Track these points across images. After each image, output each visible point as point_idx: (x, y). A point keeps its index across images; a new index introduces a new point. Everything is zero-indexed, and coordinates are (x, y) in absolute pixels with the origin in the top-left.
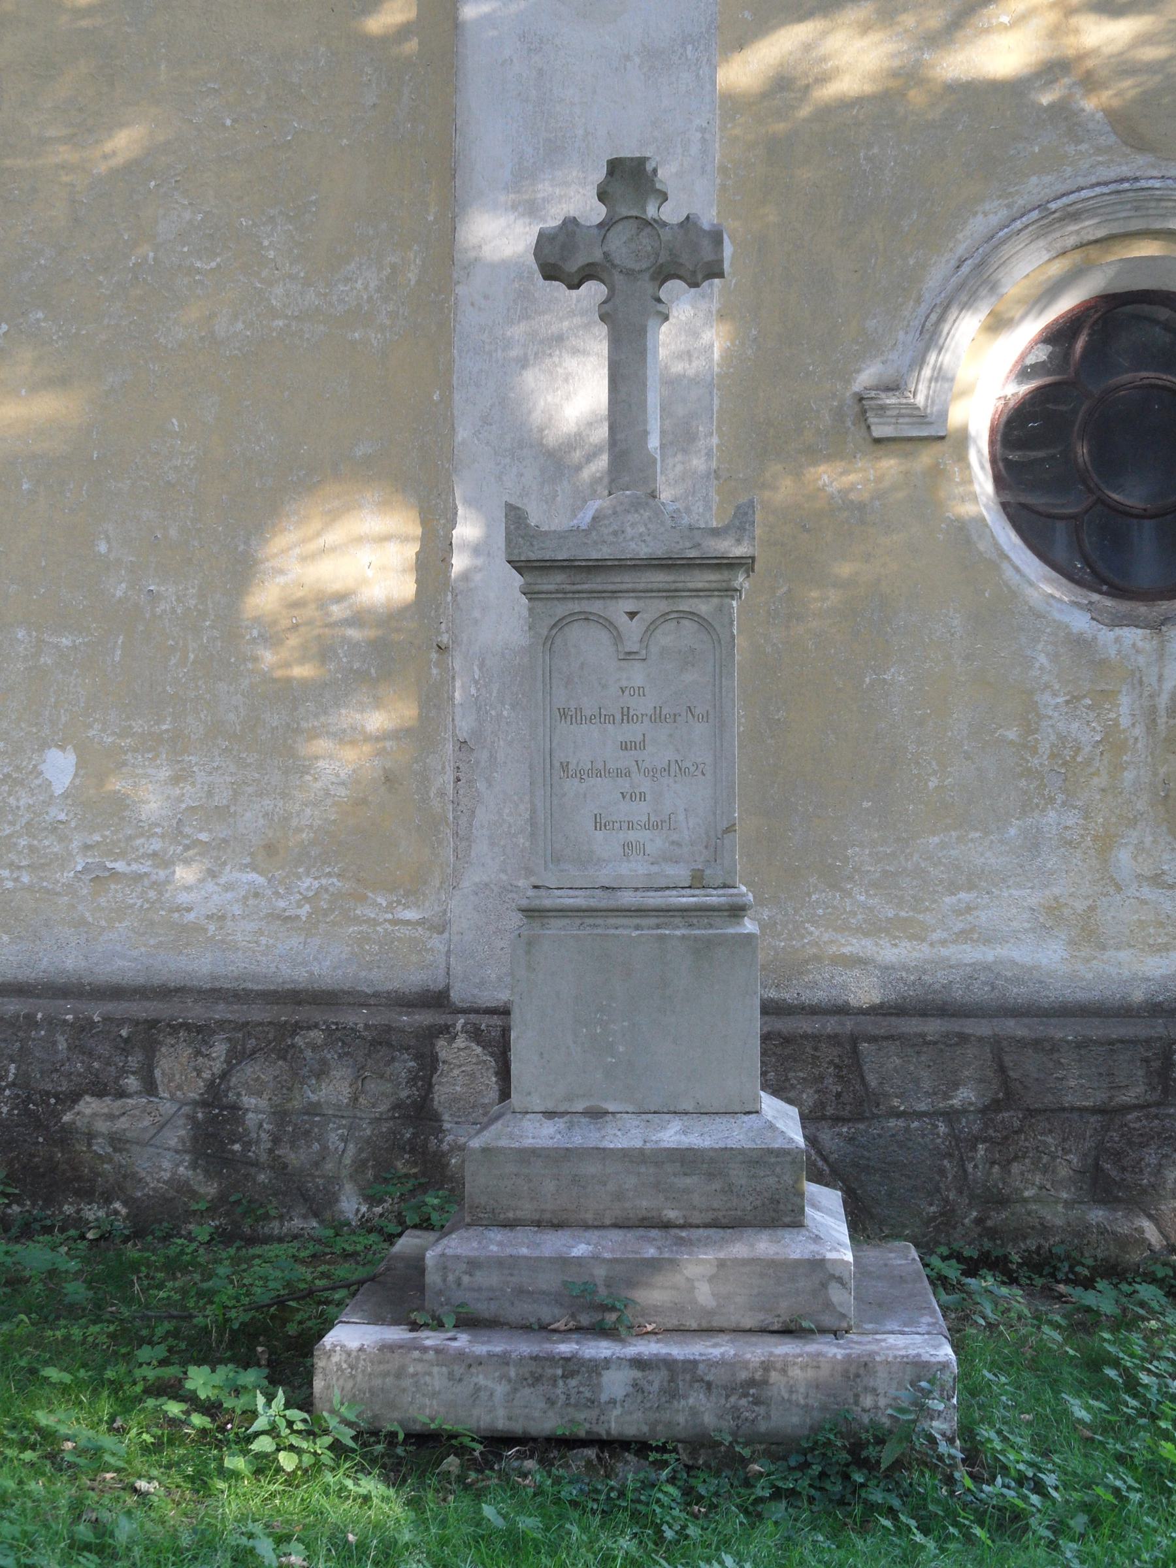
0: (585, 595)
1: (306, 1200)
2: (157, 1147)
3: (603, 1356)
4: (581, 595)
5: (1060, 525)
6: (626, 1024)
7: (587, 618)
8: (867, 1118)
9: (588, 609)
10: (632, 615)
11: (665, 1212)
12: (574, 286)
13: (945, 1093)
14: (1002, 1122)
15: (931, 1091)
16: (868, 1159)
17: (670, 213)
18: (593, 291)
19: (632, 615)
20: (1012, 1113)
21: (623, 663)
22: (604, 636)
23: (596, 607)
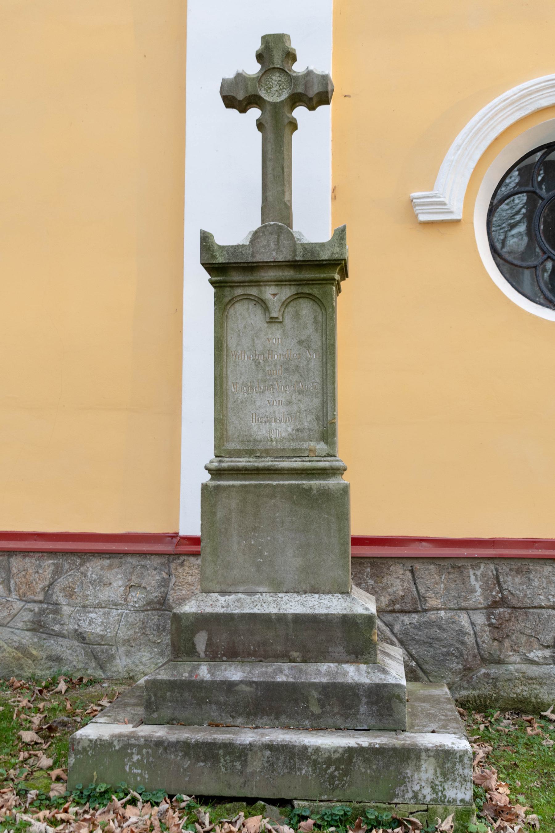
0: (247, 284)
1: (96, 659)
2: (11, 628)
3: (248, 742)
4: (245, 284)
5: (527, 273)
6: (269, 538)
7: (247, 297)
8: (419, 611)
9: (248, 292)
10: (274, 295)
11: (291, 653)
12: (243, 110)
13: (465, 597)
14: (499, 614)
15: (456, 595)
16: (420, 636)
17: (298, 68)
18: (255, 113)
19: (274, 295)
20: (505, 609)
21: (270, 325)
22: (259, 311)
23: (253, 291)
